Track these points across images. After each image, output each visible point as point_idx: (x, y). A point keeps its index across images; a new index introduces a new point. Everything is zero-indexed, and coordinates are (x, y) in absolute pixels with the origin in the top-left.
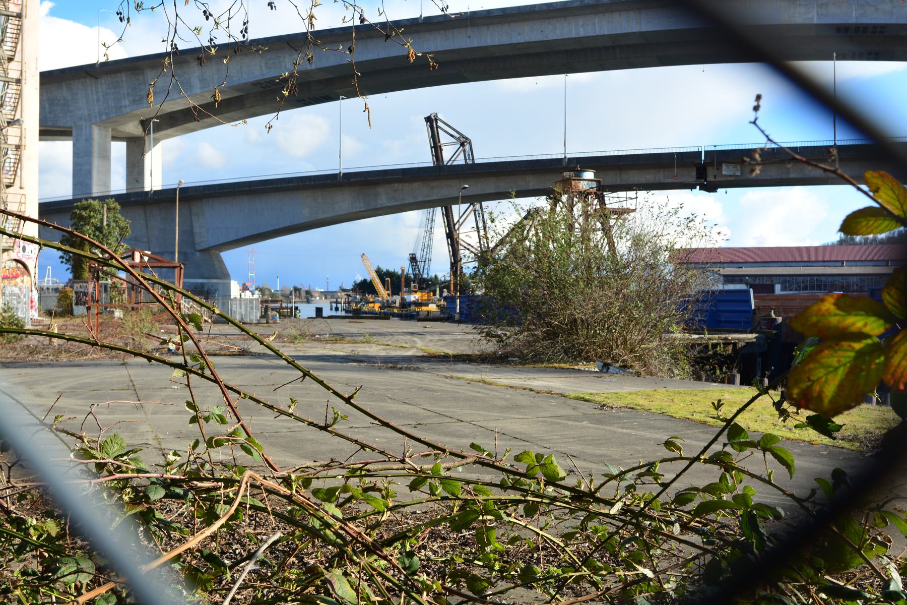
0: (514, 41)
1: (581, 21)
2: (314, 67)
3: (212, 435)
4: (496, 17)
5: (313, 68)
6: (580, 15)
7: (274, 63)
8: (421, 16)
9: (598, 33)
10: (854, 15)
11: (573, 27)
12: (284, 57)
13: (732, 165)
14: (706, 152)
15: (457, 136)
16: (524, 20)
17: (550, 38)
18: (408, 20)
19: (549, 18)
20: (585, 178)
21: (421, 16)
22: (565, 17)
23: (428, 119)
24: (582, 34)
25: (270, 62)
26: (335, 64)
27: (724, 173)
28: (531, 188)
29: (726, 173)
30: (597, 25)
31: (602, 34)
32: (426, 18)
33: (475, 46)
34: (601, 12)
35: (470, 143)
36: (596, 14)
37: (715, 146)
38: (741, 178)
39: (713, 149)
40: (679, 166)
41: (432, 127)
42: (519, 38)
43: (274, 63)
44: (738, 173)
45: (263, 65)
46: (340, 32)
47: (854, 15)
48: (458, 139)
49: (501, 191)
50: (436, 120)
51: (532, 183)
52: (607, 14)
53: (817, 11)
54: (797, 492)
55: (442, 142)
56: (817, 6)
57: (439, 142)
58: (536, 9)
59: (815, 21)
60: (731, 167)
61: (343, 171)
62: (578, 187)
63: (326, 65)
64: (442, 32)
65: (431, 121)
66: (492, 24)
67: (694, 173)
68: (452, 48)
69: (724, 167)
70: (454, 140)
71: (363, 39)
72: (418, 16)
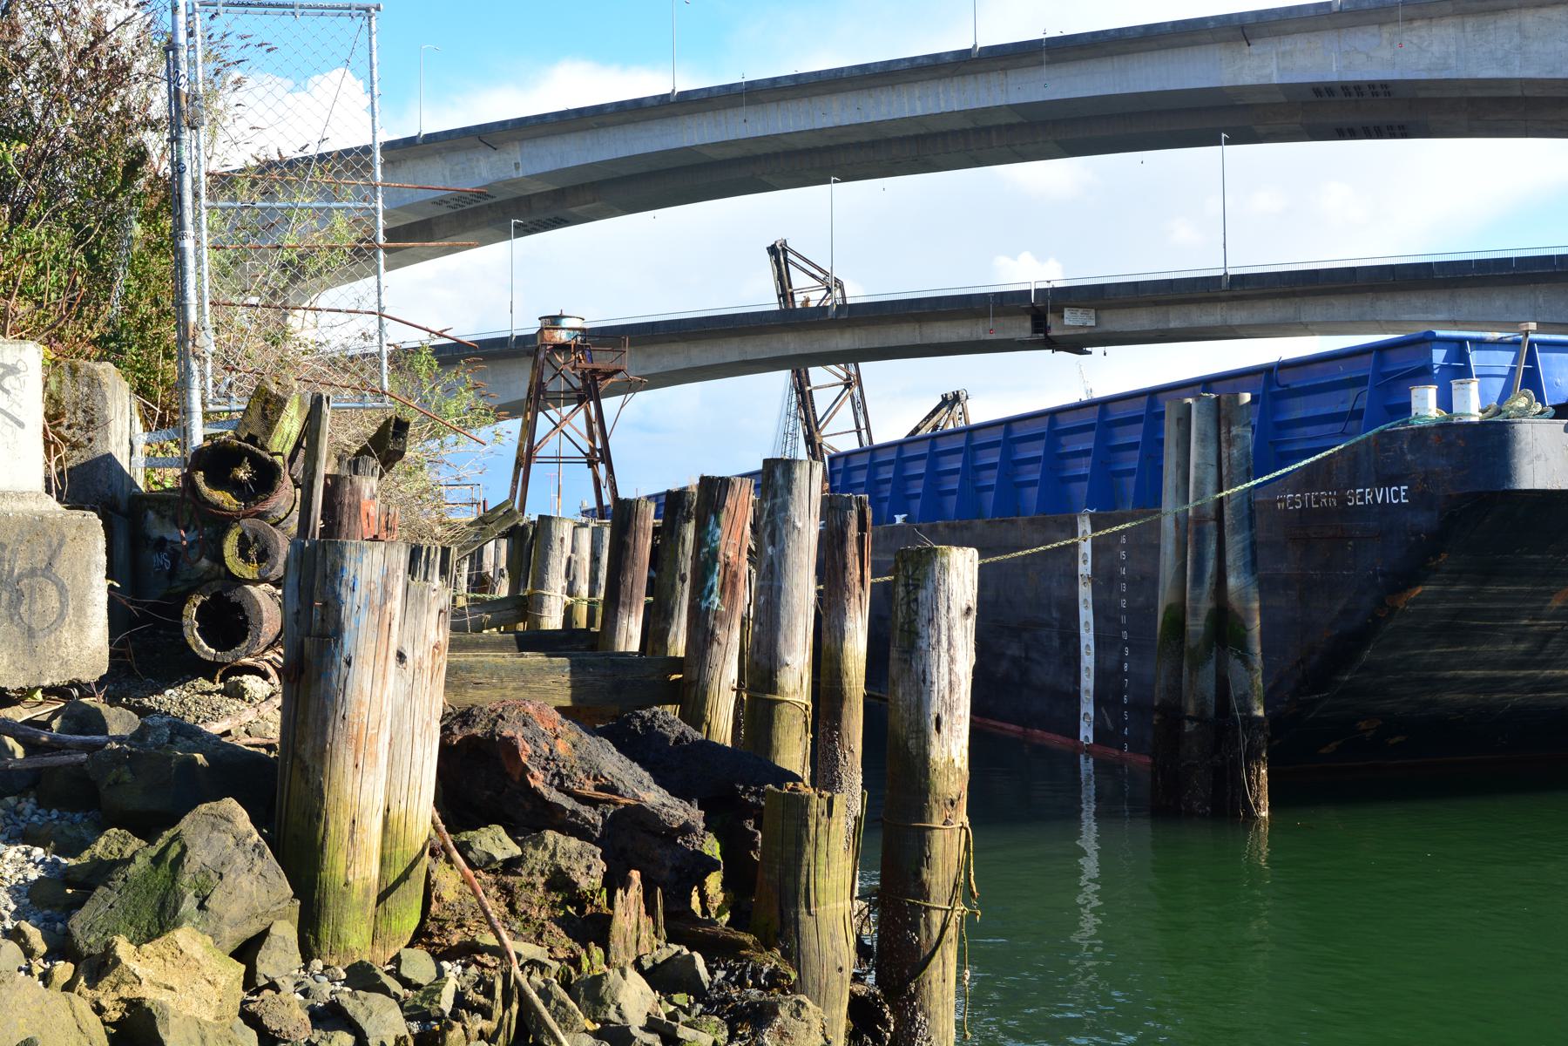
0: (818, 126)
1: (917, 90)
2: (521, 174)
3: (932, 1017)
4: (785, 88)
5: (521, 175)
6: (916, 82)
7: (463, 169)
8: (674, 91)
9: (943, 110)
10: (1334, 69)
11: (905, 100)
12: (478, 160)
13: (1081, 310)
14: (1036, 290)
15: (822, 276)
16: (832, 92)
17: (872, 119)
18: (655, 97)
19: (869, 88)
20: (563, 326)
21: (975, 46)
22: (893, 85)
23: (773, 250)
24: (919, 112)
25: (457, 168)
26: (554, 169)
27: (1067, 322)
28: (792, 352)
29: (1071, 323)
30: (941, 96)
31: (951, 110)
32: (681, 94)
33: (760, 134)
34: (947, 76)
35: (841, 287)
36: (940, 78)
37: (1049, 282)
38: (1097, 330)
39: (1045, 286)
40: (997, 314)
41: (777, 262)
42: (824, 120)
43: (463, 169)
44: (1093, 323)
45: (447, 173)
46: (554, 120)
47: (1334, 69)
48: (822, 281)
49: (749, 358)
50: (785, 251)
51: (792, 346)
52: (955, 79)
53: (1278, 63)
54: (781, 706)
55: (794, 287)
56: (1277, 54)
57: (790, 286)
58: (844, 75)
59: (1276, 80)
60: (1079, 314)
61: (516, 333)
62: (553, 337)
63: (539, 171)
64: (710, 114)
65: (778, 253)
66: (784, 99)
67: (1028, 324)
68: (725, 139)
69: (1067, 313)
70: (816, 283)
71: (593, 128)
72: (669, 91)
